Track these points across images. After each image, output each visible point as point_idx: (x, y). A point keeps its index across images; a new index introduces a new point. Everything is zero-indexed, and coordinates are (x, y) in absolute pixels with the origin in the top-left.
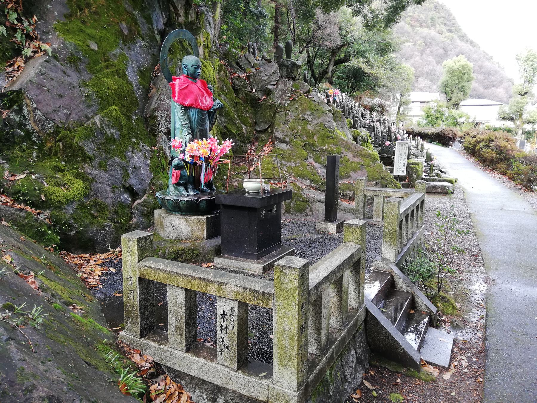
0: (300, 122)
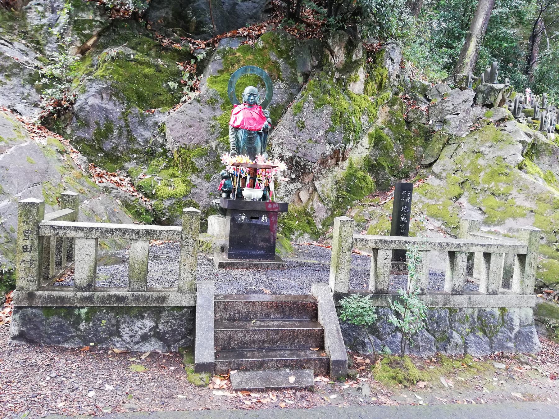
0: (472, 154)
